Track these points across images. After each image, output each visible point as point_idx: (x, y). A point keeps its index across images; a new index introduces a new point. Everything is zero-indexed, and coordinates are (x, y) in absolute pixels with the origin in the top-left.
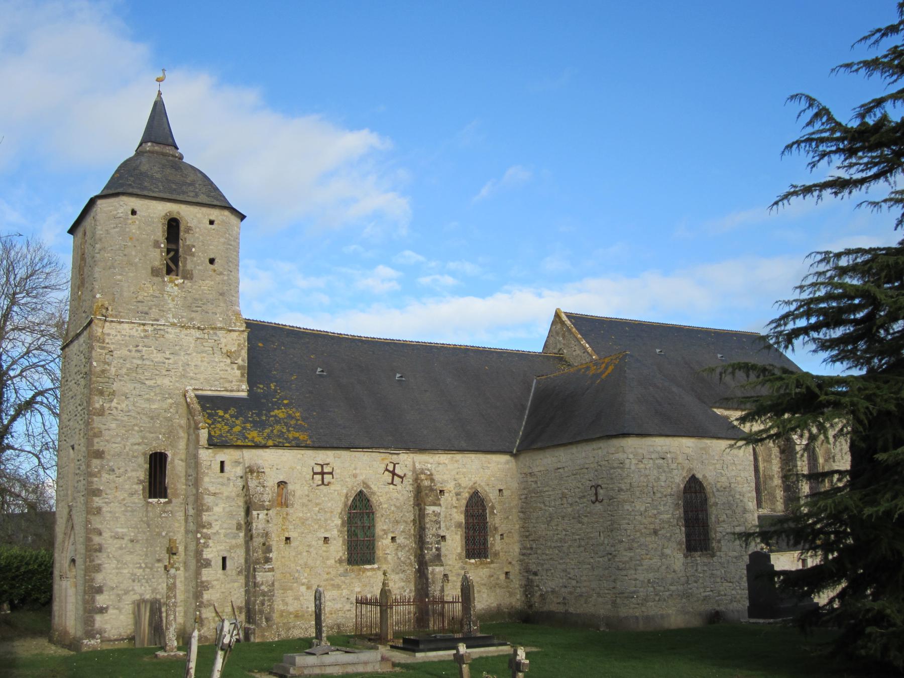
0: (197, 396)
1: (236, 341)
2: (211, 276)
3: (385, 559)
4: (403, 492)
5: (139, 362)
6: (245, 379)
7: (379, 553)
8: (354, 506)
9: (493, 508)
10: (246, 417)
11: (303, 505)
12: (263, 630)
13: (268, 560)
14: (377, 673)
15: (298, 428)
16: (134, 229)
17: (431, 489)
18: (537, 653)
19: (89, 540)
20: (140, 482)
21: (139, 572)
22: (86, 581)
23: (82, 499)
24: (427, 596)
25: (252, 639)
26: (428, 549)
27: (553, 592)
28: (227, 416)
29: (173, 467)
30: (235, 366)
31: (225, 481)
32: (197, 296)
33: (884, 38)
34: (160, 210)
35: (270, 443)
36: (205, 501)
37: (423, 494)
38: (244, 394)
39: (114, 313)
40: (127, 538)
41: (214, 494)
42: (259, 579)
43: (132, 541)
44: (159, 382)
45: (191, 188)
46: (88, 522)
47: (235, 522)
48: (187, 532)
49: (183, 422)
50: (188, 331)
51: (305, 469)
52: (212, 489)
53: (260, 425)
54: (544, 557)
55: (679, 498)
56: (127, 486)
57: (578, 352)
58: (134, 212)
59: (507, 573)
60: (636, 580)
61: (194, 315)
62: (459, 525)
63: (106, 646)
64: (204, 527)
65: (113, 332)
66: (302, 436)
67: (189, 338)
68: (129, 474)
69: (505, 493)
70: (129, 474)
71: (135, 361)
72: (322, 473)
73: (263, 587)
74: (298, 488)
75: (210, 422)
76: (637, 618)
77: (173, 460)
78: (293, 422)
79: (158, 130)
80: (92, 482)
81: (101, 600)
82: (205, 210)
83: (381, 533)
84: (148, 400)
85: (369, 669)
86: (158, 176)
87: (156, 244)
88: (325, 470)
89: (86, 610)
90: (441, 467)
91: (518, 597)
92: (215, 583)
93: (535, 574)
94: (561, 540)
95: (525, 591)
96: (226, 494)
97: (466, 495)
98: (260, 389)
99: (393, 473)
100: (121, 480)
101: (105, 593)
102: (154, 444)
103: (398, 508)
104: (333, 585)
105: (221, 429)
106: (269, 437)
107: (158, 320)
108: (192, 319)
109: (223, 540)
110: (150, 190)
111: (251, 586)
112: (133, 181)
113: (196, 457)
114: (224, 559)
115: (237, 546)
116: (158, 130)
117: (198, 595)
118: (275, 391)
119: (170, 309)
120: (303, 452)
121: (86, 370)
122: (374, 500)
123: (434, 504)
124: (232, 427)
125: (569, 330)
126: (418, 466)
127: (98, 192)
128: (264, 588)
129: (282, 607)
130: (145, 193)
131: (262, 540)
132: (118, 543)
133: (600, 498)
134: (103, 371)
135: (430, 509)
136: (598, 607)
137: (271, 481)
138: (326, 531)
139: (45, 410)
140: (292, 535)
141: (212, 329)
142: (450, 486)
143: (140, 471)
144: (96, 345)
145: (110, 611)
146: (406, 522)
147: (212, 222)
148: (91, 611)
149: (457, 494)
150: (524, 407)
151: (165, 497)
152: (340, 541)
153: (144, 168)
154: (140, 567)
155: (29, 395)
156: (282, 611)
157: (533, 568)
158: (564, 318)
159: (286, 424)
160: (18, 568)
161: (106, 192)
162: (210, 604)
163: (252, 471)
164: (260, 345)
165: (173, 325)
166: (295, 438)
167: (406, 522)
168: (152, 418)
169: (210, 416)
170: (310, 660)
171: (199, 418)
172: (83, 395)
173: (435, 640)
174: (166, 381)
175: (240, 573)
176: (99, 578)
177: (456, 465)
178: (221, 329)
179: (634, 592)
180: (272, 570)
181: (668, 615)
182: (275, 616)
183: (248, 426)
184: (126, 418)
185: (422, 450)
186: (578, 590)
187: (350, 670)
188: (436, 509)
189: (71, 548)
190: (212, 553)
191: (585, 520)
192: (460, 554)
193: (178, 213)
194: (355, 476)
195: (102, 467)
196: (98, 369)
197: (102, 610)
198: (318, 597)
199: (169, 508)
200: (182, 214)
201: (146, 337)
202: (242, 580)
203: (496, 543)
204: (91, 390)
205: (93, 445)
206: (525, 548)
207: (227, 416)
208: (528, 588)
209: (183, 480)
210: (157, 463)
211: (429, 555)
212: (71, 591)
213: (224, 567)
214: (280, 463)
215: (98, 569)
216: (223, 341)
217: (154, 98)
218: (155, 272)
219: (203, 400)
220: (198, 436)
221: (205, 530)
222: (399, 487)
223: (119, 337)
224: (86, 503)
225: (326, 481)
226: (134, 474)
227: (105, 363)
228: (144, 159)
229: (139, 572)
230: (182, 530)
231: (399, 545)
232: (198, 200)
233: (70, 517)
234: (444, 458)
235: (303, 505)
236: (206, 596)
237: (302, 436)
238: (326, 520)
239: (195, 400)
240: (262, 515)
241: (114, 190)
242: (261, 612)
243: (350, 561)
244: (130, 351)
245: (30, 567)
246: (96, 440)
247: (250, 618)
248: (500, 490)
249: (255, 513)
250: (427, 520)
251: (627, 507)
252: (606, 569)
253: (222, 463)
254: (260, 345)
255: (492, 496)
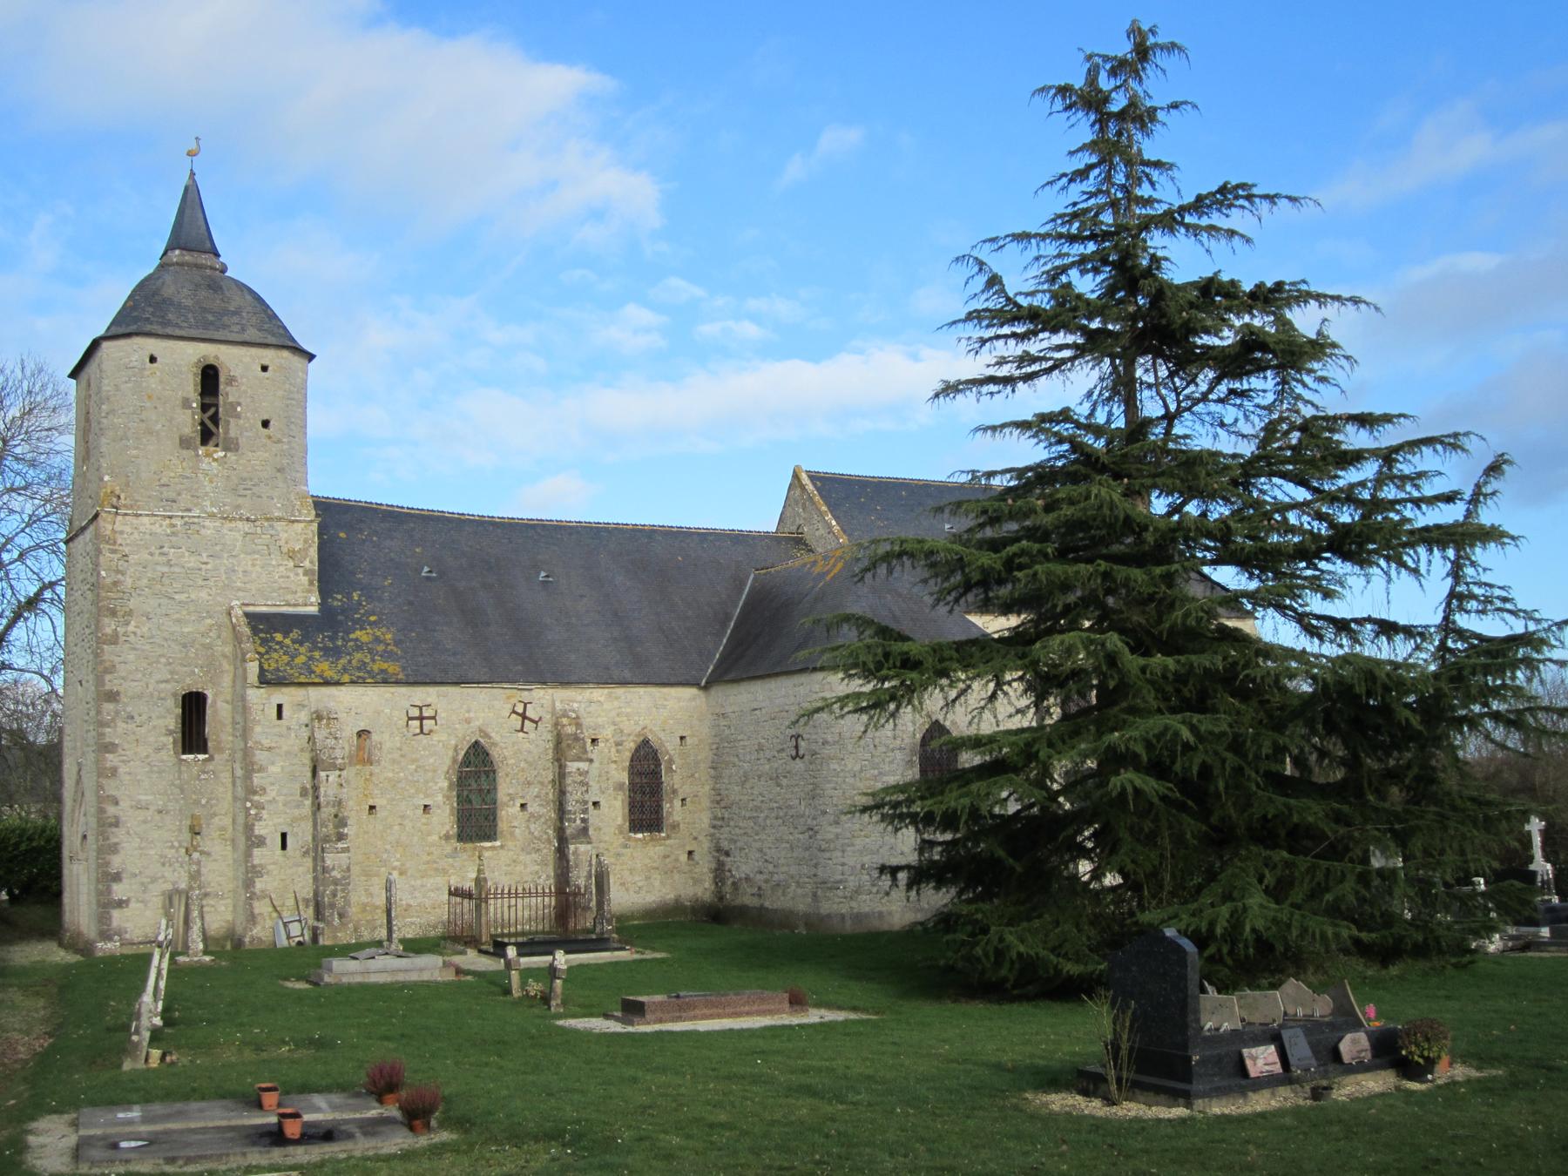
0: (247, 615)
1: (303, 534)
2: (264, 445)
3: (512, 834)
4: (538, 742)
5: (165, 569)
6: (316, 588)
7: (502, 825)
8: (466, 762)
9: (671, 761)
10: (314, 643)
11: (394, 761)
12: (336, 929)
13: (341, 837)
14: (436, 982)
15: (388, 656)
16: (153, 383)
17: (576, 738)
18: (662, 961)
19: (101, 811)
20: (170, 733)
21: (171, 853)
22: (99, 866)
23: (91, 757)
24: (567, 883)
25: (321, 942)
26: (569, 820)
27: (747, 879)
28: (287, 641)
29: (215, 712)
30: (300, 571)
31: (284, 731)
32: (245, 475)
33: (1073, 185)
34: (192, 353)
35: (346, 678)
36: (256, 759)
37: (566, 745)
38: (313, 610)
39: (128, 502)
40: (152, 808)
41: (269, 749)
42: (328, 862)
43: (160, 812)
44: (193, 596)
45: (235, 319)
46: (100, 787)
47: (297, 786)
48: (235, 798)
49: (228, 649)
50: (233, 525)
51: (396, 713)
52: (266, 742)
53: (333, 653)
54: (737, 831)
55: (913, 752)
56: (152, 739)
57: (822, 531)
58: (153, 359)
59: (690, 853)
60: (843, 864)
61: (240, 501)
62: (620, 787)
63: (128, 951)
64: (255, 793)
65: (128, 529)
66: (392, 668)
67: (234, 533)
68: (155, 722)
69: (689, 740)
70: (155, 722)
71: (159, 568)
72: (421, 718)
73: (335, 873)
74: (386, 740)
75: (262, 650)
76: (843, 916)
77: (214, 702)
78: (381, 648)
79: (191, 235)
80: (103, 734)
81: (119, 891)
82: (254, 351)
83: (506, 799)
84: (178, 621)
85: (426, 977)
86: (188, 302)
87: (186, 404)
88: (426, 714)
89: (99, 904)
90: (593, 708)
91: (707, 885)
92: (270, 867)
93: (727, 854)
94: (757, 809)
95: (716, 877)
96: (285, 748)
97: (631, 746)
98: (337, 601)
99: (524, 716)
100: (143, 730)
101: (125, 881)
102: (188, 681)
103: (530, 764)
104: (436, 869)
105: (278, 660)
106: (345, 670)
107: (189, 510)
108: (238, 507)
109: (281, 808)
110: (177, 326)
111: (320, 872)
112: (153, 314)
113: (243, 698)
114: (284, 836)
115: (302, 819)
116: (191, 235)
117: (249, 884)
118: (359, 603)
119: (207, 494)
120: (392, 689)
121: (93, 580)
122: (495, 753)
123: (579, 759)
124: (293, 657)
125: (811, 499)
126: (558, 706)
127: (101, 332)
128: (336, 874)
129: (364, 899)
130: (169, 331)
131: (333, 811)
132: (142, 815)
133: (801, 752)
134: (115, 583)
135: (572, 766)
136: (795, 900)
137: (349, 730)
138: (427, 796)
139: (54, 611)
140: (378, 802)
141: (267, 519)
142: (607, 733)
143: (170, 717)
144: (105, 547)
145: (133, 905)
146: (542, 783)
147: (264, 369)
148: (107, 905)
149: (618, 744)
150: (728, 618)
151: (205, 752)
152: (447, 809)
153: (169, 291)
154: (172, 847)
155: (33, 590)
156: (365, 905)
157: (725, 845)
158: (804, 477)
159: (370, 651)
160: (17, 845)
161: (114, 331)
162: (264, 895)
163: (319, 718)
164: (342, 535)
165: (212, 515)
166: (383, 671)
167: (542, 783)
168: (185, 646)
169: (264, 642)
170: (352, 965)
171: (248, 646)
172: (96, 608)
173: (576, 941)
174: (204, 594)
175: (306, 853)
176: (116, 862)
177: (616, 703)
178: (280, 519)
179: (840, 882)
180: (347, 850)
181: (890, 913)
182: (353, 911)
183: (317, 654)
184: (148, 647)
185: (565, 683)
186: (776, 877)
187: (401, 977)
188: (583, 766)
189: (82, 819)
190: (267, 828)
191: (784, 782)
192: (620, 827)
193: (216, 357)
194: (468, 721)
195: (117, 713)
196: (108, 581)
197: (121, 904)
198: (389, 887)
199: (210, 767)
200: (222, 358)
201: (173, 534)
202: (309, 862)
203: (673, 810)
204: (99, 609)
205: (103, 684)
206: (715, 818)
207: (287, 641)
208: (719, 872)
209: (229, 729)
210: (193, 707)
211: (571, 828)
212: (84, 879)
213: (284, 846)
214: (357, 705)
215: (114, 849)
216: (284, 536)
217: (185, 180)
218: (185, 443)
219: (254, 619)
220: (245, 670)
221: (256, 798)
222: (532, 735)
223: (136, 535)
224: (97, 761)
225: (426, 730)
226: (161, 722)
227: (118, 572)
228: (168, 278)
229: (171, 853)
230: (229, 795)
231: (532, 815)
232: (246, 337)
233: (79, 781)
234: (599, 694)
235: (394, 761)
236: (259, 885)
237: (392, 668)
238: (427, 782)
239: (243, 620)
240: (333, 776)
241: (128, 324)
242: (332, 906)
243: (463, 836)
244: (151, 554)
245: (34, 844)
246: (108, 677)
247: (319, 914)
248: (682, 738)
249: (322, 774)
250: (569, 780)
251: (834, 765)
252: (807, 849)
253: (280, 707)
254: (342, 535)
255: (668, 745)
